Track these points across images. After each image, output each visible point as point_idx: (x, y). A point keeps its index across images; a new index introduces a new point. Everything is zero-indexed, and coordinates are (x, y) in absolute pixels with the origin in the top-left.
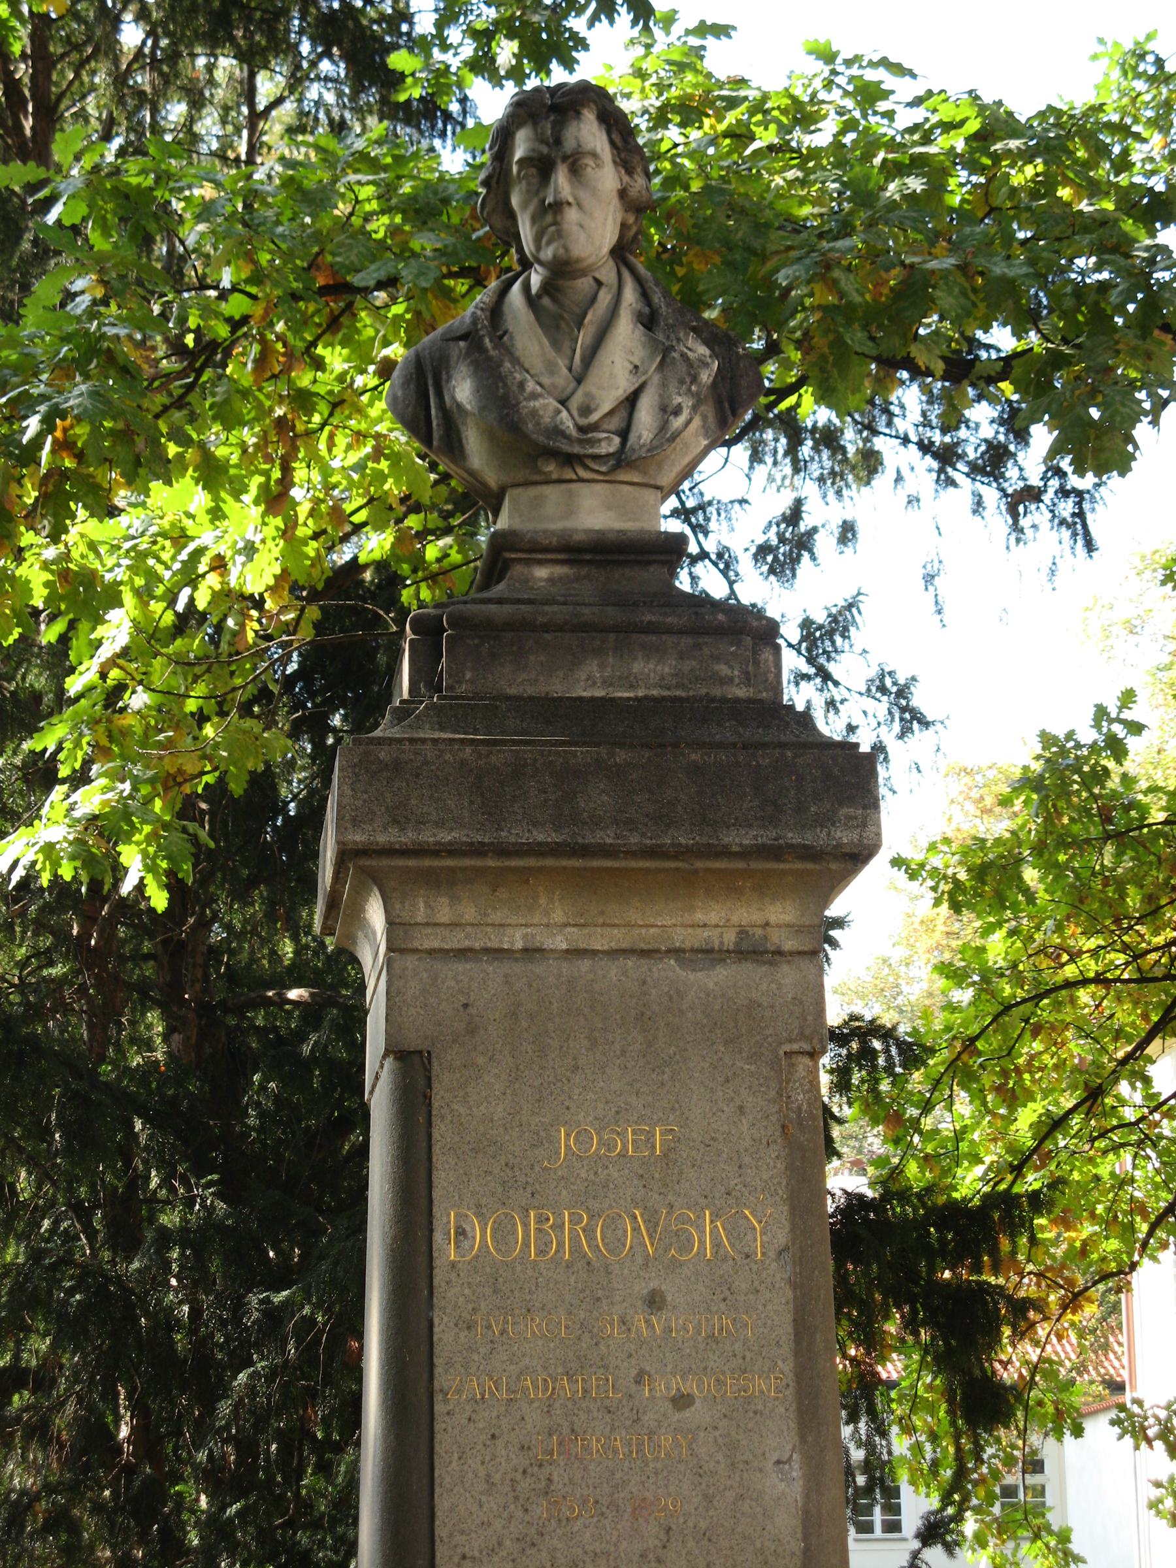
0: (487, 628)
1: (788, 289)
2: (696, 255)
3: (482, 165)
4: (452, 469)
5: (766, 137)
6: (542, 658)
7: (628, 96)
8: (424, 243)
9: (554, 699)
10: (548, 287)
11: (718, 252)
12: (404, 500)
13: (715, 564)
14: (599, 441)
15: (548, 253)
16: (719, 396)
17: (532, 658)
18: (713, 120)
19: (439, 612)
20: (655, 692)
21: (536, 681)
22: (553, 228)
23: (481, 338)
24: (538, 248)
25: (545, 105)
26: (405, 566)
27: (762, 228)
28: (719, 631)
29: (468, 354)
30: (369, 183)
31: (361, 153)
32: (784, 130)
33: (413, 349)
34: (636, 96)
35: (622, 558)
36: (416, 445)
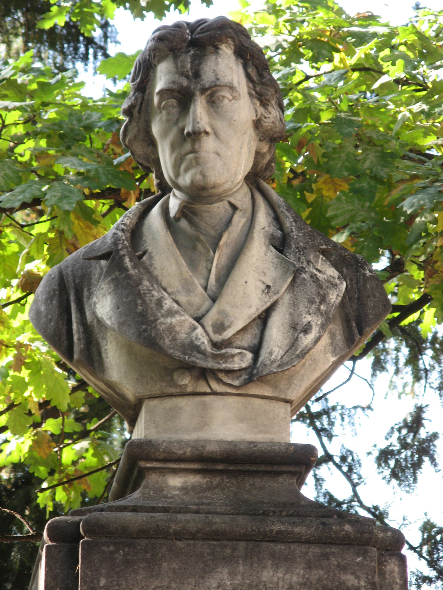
0: (123, 536)
1: (413, 217)
2: (325, 182)
3: (124, 95)
4: (89, 378)
5: (395, 71)
6: (174, 565)
7: (262, 31)
8: (67, 167)
10: (186, 211)
11: (346, 180)
12: (43, 405)
13: (339, 467)
14: (233, 356)
15: (186, 179)
16: (347, 315)
17: (165, 565)
18: (343, 55)
19: (77, 518)
22: (191, 156)
23: (122, 258)
24: (177, 175)
25: (185, 40)
26: (42, 469)
27: (387, 158)
28: (346, 542)
29: (109, 273)
30: (15, 109)
31: (8, 80)
32: (410, 65)
33: (56, 267)
34: (271, 31)
35: (253, 468)
36: (55, 353)
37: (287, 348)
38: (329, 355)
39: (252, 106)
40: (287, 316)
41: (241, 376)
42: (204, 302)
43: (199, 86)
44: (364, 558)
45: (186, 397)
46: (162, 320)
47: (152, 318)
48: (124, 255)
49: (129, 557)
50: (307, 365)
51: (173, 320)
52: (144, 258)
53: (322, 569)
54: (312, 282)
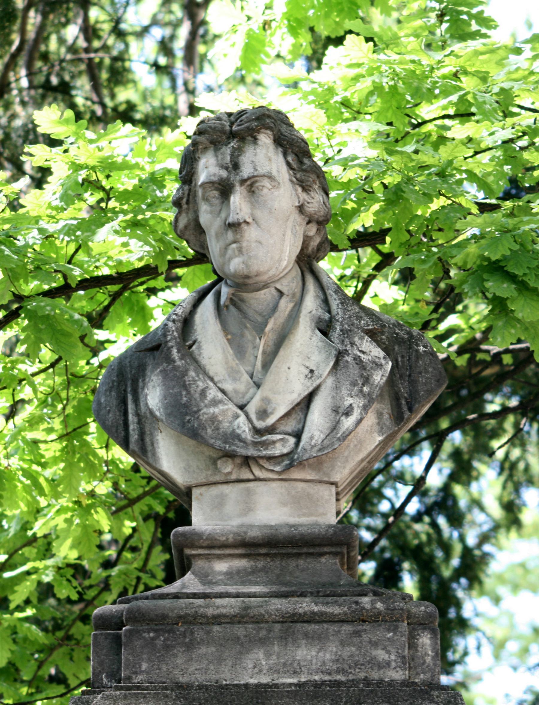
9: (222, 687)
14: (274, 442)
20: (317, 678)
21: (207, 669)
22: (234, 246)
23: (170, 349)
37: (328, 432)
38: (376, 435)
39: (294, 193)
40: (330, 400)
41: (283, 461)
42: (249, 389)
43: (238, 178)
44: (395, 633)
45: (231, 484)
46: (205, 410)
47: (195, 409)
48: (172, 347)
49: (169, 642)
50: (352, 446)
51: (215, 410)
52: (194, 347)
53: (354, 646)
54: (355, 365)
